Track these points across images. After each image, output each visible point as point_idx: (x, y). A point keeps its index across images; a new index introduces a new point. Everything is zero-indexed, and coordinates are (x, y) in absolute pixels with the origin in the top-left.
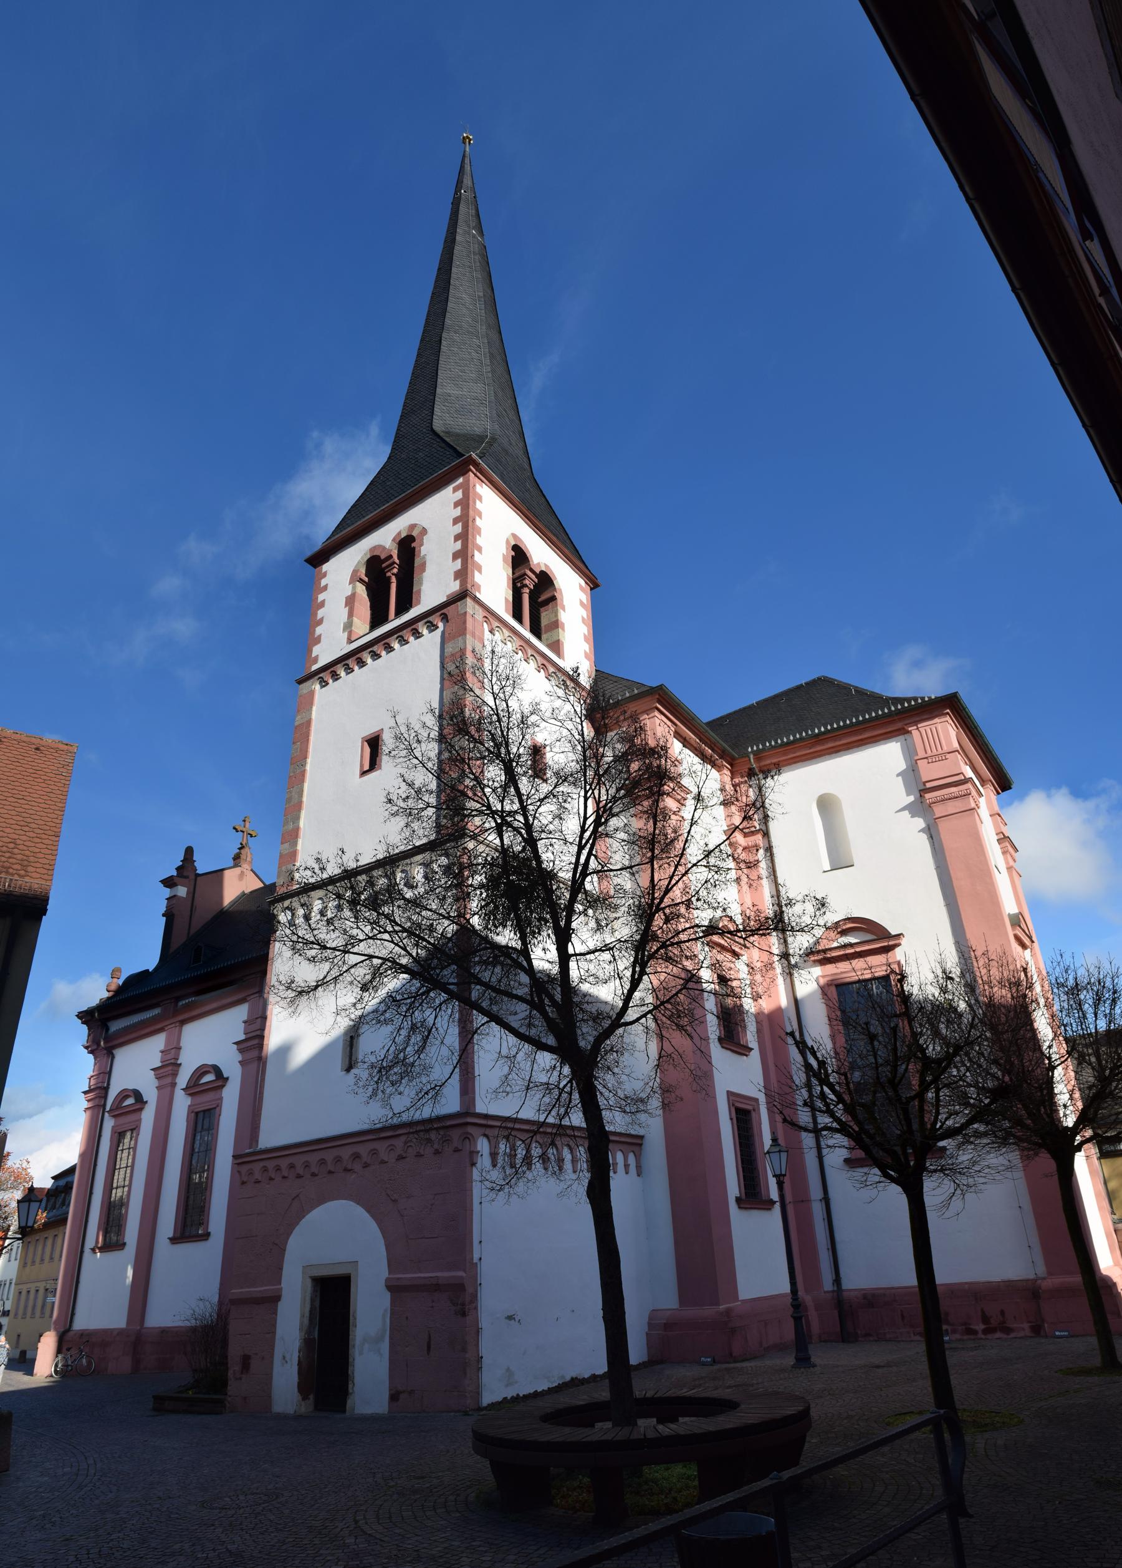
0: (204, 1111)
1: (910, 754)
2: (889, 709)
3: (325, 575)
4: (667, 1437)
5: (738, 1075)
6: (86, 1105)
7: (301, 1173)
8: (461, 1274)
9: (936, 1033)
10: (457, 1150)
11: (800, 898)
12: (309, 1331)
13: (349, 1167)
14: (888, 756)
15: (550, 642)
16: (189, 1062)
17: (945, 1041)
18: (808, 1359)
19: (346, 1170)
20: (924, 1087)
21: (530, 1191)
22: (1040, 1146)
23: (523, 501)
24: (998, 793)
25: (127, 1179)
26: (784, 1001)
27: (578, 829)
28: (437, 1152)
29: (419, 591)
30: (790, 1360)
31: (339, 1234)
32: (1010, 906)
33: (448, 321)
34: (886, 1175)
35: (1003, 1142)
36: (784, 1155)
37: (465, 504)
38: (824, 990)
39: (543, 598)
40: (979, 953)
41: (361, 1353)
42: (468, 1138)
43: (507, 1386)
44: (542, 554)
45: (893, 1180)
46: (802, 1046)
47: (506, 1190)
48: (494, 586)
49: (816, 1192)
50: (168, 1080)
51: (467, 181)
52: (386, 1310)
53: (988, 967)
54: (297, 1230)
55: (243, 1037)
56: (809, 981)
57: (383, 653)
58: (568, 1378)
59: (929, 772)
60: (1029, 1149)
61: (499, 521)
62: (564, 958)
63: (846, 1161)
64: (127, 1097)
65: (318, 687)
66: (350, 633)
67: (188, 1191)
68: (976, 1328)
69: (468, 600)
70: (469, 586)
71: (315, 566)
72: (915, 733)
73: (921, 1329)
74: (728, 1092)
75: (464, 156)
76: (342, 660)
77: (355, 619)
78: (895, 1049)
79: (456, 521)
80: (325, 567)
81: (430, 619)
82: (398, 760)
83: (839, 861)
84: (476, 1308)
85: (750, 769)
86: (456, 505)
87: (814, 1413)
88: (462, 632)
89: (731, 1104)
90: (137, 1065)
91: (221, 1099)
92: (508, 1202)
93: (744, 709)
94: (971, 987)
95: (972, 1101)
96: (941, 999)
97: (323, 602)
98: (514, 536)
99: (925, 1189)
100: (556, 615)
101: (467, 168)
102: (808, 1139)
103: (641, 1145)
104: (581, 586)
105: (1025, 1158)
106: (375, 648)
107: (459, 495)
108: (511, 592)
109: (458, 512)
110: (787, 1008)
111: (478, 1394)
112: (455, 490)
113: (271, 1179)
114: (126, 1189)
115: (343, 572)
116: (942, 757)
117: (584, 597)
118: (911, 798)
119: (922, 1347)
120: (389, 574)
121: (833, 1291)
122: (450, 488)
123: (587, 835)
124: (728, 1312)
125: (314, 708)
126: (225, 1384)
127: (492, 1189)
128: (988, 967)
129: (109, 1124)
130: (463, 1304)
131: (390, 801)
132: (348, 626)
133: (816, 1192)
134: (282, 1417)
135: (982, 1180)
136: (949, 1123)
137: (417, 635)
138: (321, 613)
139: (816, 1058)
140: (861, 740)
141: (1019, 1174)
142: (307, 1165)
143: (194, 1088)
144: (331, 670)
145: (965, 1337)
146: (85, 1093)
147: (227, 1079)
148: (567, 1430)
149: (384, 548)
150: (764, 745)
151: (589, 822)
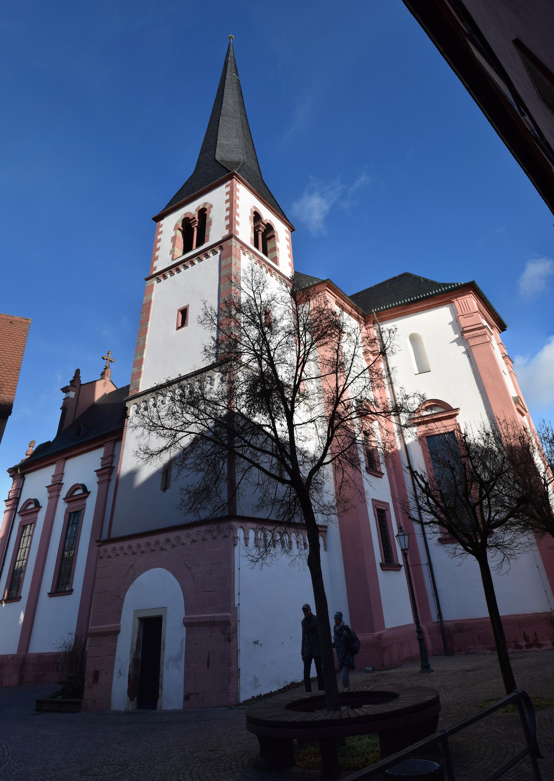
0: (75, 512)
1: (454, 312)
2: (441, 289)
3: (161, 226)
4: (362, 716)
5: (378, 489)
6: (5, 508)
7: (135, 551)
8: (228, 614)
9: (485, 467)
10: (226, 536)
11: (412, 395)
12: (136, 654)
13: (164, 547)
14: (443, 314)
15: (272, 257)
16: (68, 483)
17: (490, 472)
18: (428, 666)
19: (162, 549)
20: (482, 498)
21: (273, 562)
22: (546, 530)
23: (258, 191)
24: (500, 333)
25: (26, 555)
26: (399, 446)
27: (296, 359)
28: (214, 538)
29: (208, 235)
30: (417, 668)
31: (155, 590)
32: (513, 393)
33: (222, 112)
34: (467, 550)
35: (525, 528)
36: (406, 537)
37: (231, 193)
38: (420, 439)
39: (268, 236)
40: (501, 421)
41: (167, 668)
42: (232, 529)
43: (254, 688)
44: (267, 215)
45: (470, 552)
46: (413, 474)
47: (260, 561)
48: (245, 232)
49: (424, 560)
50: (55, 493)
51: (231, 54)
52: (183, 639)
53: (507, 428)
54: (131, 587)
55: (100, 467)
56: (411, 436)
57: (190, 266)
58: (289, 683)
59: (465, 322)
60: (539, 532)
61: (247, 201)
62: (291, 427)
63: (440, 540)
64: (30, 504)
65: (156, 282)
66: (173, 255)
67: (62, 563)
68: (521, 644)
69: (233, 239)
70: (233, 232)
71: (157, 222)
72: (456, 303)
73: (494, 645)
74: (372, 499)
75: (230, 44)
76: (169, 269)
77: (176, 248)
78: (466, 476)
79: (227, 202)
80: (162, 222)
81: (214, 248)
82: (206, 326)
83: (423, 369)
84: (236, 637)
85: (374, 320)
86: (227, 194)
87: (441, 699)
88: (230, 254)
89: (374, 507)
90: (38, 484)
91: (85, 505)
92: (261, 569)
93: (368, 289)
94: (498, 439)
95: (506, 504)
96: (485, 447)
97: (160, 239)
98: (254, 207)
99: (488, 558)
100: (275, 244)
101: (231, 49)
102: (417, 527)
103: (326, 532)
104: (286, 231)
105: (539, 538)
106: (185, 263)
107: (228, 189)
108: (253, 234)
109: (228, 197)
110: (401, 450)
111: (237, 694)
112: (226, 187)
113: (118, 555)
114: (25, 561)
115: (170, 225)
116: (470, 315)
117: (288, 236)
118: (457, 336)
119: (496, 657)
120: (193, 226)
121: (438, 622)
122: (224, 186)
123: (300, 360)
124: (380, 636)
125: (153, 293)
126: (82, 691)
127: (252, 561)
128: (507, 428)
129: (18, 520)
130: (229, 634)
131: (206, 350)
132: (172, 252)
133: (424, 560)
134: (117, 713)
135: (517, 551)
136: (497, 517)
137: (207, 256)
138: (158, 245)
139: (423, 481)
140: (430, 306)
141: (535, 548)
142: (139, 546)
143: (70, 498)
144: (163, 273)
145: (516, 651)
146: (6, 501)
147: (90, 492)
148: (303, 714)
149: (191, 214)
150: (380, 308)
151: (301, 353)
